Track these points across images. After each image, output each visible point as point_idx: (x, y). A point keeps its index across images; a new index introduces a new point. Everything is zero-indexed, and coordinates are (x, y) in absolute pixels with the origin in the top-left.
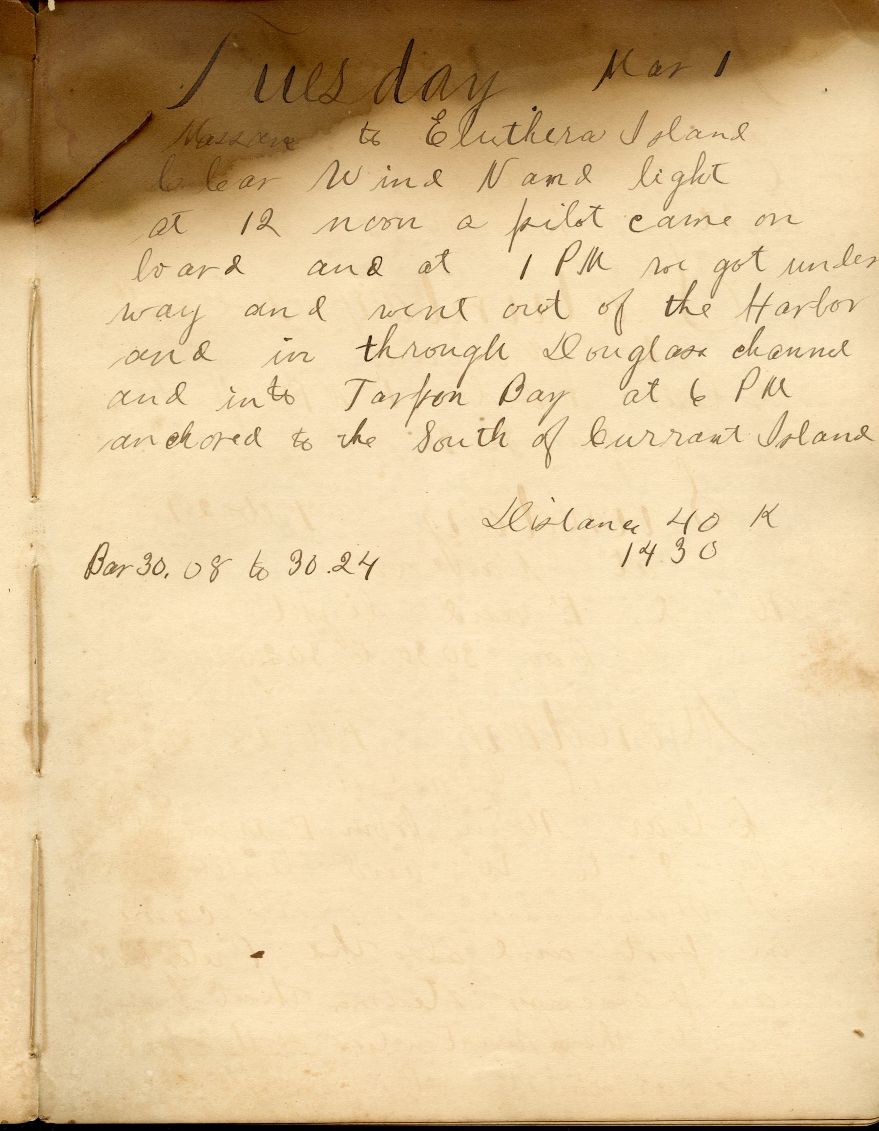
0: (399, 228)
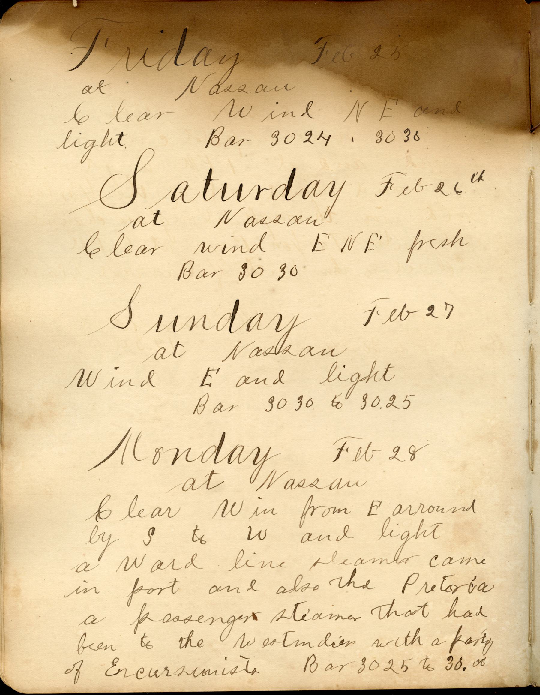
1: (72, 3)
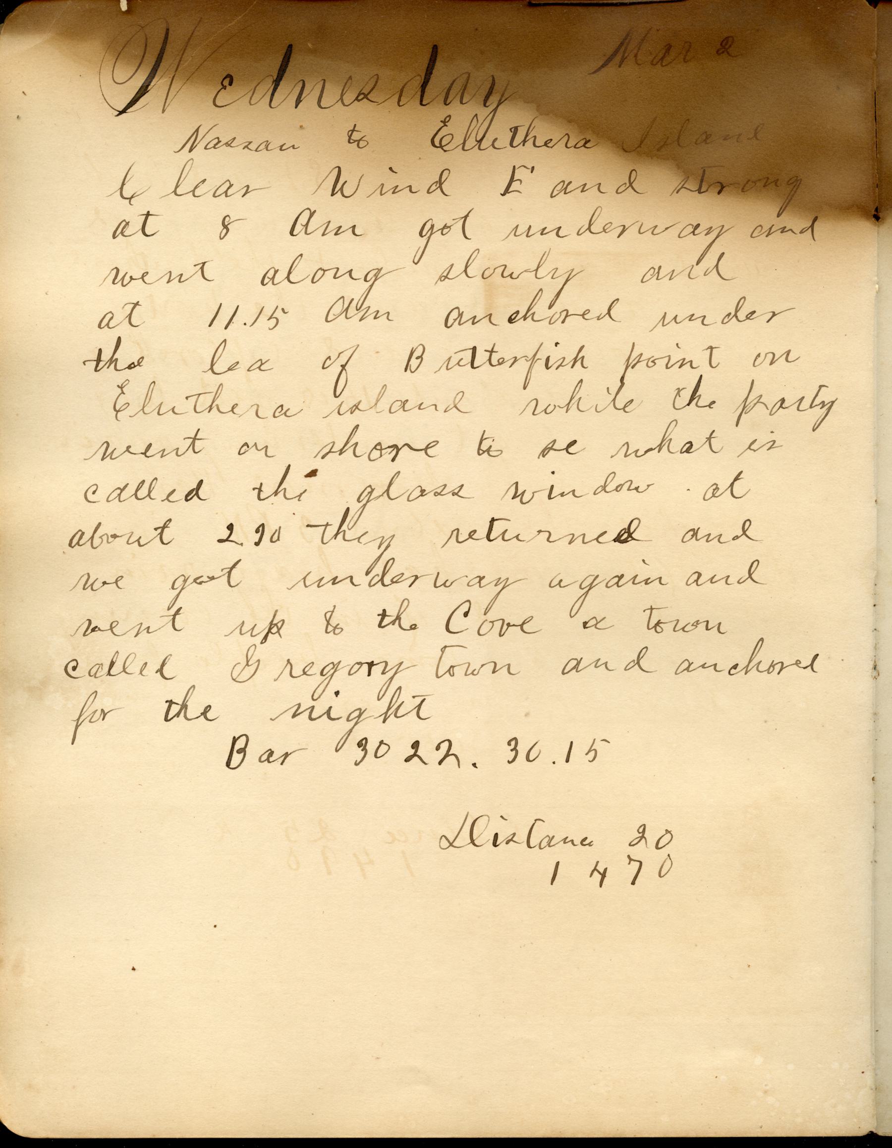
1: (119, 4)
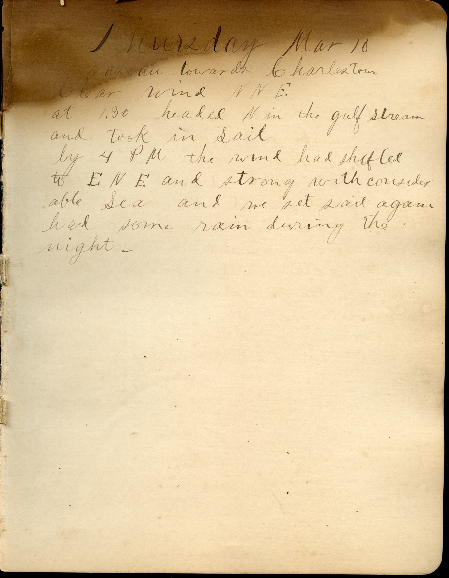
0: (183, 91)
1: (60, 3)
